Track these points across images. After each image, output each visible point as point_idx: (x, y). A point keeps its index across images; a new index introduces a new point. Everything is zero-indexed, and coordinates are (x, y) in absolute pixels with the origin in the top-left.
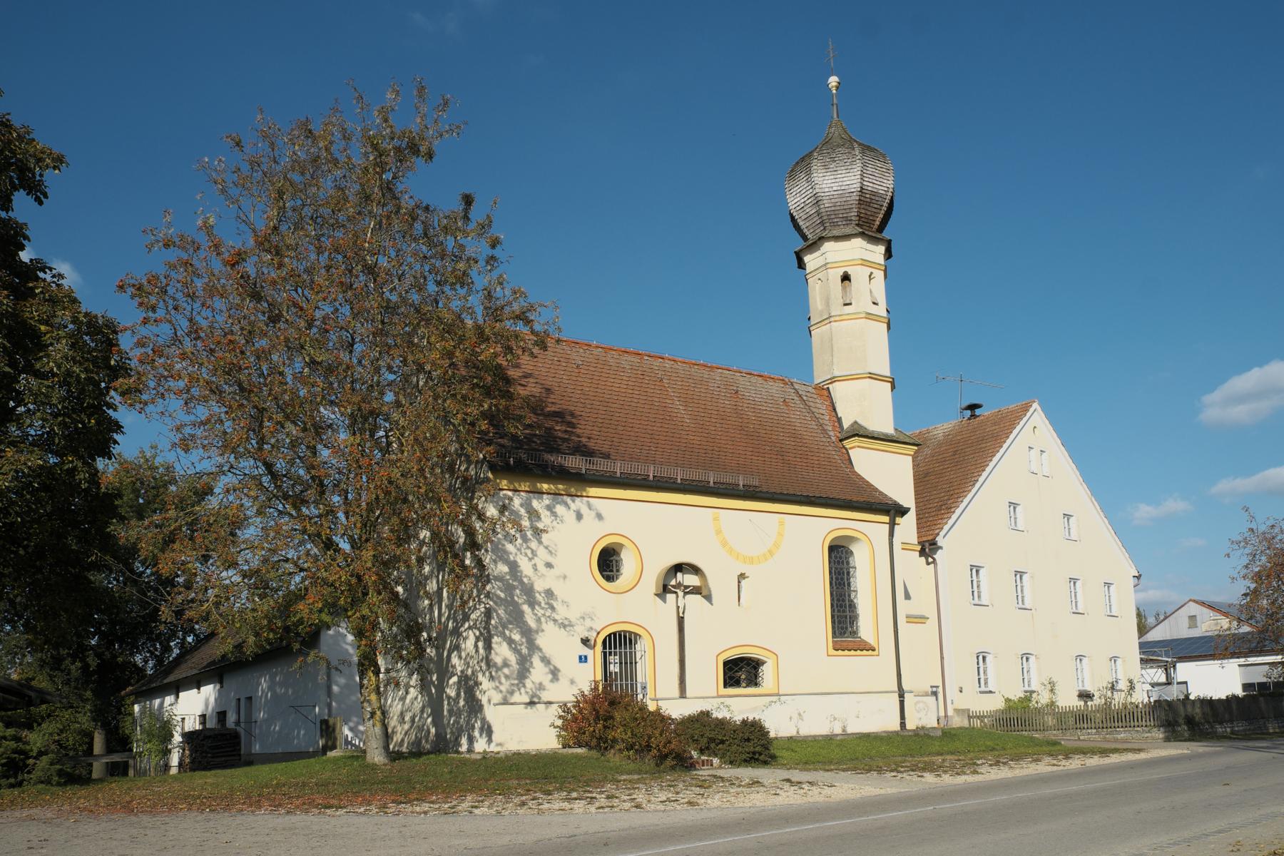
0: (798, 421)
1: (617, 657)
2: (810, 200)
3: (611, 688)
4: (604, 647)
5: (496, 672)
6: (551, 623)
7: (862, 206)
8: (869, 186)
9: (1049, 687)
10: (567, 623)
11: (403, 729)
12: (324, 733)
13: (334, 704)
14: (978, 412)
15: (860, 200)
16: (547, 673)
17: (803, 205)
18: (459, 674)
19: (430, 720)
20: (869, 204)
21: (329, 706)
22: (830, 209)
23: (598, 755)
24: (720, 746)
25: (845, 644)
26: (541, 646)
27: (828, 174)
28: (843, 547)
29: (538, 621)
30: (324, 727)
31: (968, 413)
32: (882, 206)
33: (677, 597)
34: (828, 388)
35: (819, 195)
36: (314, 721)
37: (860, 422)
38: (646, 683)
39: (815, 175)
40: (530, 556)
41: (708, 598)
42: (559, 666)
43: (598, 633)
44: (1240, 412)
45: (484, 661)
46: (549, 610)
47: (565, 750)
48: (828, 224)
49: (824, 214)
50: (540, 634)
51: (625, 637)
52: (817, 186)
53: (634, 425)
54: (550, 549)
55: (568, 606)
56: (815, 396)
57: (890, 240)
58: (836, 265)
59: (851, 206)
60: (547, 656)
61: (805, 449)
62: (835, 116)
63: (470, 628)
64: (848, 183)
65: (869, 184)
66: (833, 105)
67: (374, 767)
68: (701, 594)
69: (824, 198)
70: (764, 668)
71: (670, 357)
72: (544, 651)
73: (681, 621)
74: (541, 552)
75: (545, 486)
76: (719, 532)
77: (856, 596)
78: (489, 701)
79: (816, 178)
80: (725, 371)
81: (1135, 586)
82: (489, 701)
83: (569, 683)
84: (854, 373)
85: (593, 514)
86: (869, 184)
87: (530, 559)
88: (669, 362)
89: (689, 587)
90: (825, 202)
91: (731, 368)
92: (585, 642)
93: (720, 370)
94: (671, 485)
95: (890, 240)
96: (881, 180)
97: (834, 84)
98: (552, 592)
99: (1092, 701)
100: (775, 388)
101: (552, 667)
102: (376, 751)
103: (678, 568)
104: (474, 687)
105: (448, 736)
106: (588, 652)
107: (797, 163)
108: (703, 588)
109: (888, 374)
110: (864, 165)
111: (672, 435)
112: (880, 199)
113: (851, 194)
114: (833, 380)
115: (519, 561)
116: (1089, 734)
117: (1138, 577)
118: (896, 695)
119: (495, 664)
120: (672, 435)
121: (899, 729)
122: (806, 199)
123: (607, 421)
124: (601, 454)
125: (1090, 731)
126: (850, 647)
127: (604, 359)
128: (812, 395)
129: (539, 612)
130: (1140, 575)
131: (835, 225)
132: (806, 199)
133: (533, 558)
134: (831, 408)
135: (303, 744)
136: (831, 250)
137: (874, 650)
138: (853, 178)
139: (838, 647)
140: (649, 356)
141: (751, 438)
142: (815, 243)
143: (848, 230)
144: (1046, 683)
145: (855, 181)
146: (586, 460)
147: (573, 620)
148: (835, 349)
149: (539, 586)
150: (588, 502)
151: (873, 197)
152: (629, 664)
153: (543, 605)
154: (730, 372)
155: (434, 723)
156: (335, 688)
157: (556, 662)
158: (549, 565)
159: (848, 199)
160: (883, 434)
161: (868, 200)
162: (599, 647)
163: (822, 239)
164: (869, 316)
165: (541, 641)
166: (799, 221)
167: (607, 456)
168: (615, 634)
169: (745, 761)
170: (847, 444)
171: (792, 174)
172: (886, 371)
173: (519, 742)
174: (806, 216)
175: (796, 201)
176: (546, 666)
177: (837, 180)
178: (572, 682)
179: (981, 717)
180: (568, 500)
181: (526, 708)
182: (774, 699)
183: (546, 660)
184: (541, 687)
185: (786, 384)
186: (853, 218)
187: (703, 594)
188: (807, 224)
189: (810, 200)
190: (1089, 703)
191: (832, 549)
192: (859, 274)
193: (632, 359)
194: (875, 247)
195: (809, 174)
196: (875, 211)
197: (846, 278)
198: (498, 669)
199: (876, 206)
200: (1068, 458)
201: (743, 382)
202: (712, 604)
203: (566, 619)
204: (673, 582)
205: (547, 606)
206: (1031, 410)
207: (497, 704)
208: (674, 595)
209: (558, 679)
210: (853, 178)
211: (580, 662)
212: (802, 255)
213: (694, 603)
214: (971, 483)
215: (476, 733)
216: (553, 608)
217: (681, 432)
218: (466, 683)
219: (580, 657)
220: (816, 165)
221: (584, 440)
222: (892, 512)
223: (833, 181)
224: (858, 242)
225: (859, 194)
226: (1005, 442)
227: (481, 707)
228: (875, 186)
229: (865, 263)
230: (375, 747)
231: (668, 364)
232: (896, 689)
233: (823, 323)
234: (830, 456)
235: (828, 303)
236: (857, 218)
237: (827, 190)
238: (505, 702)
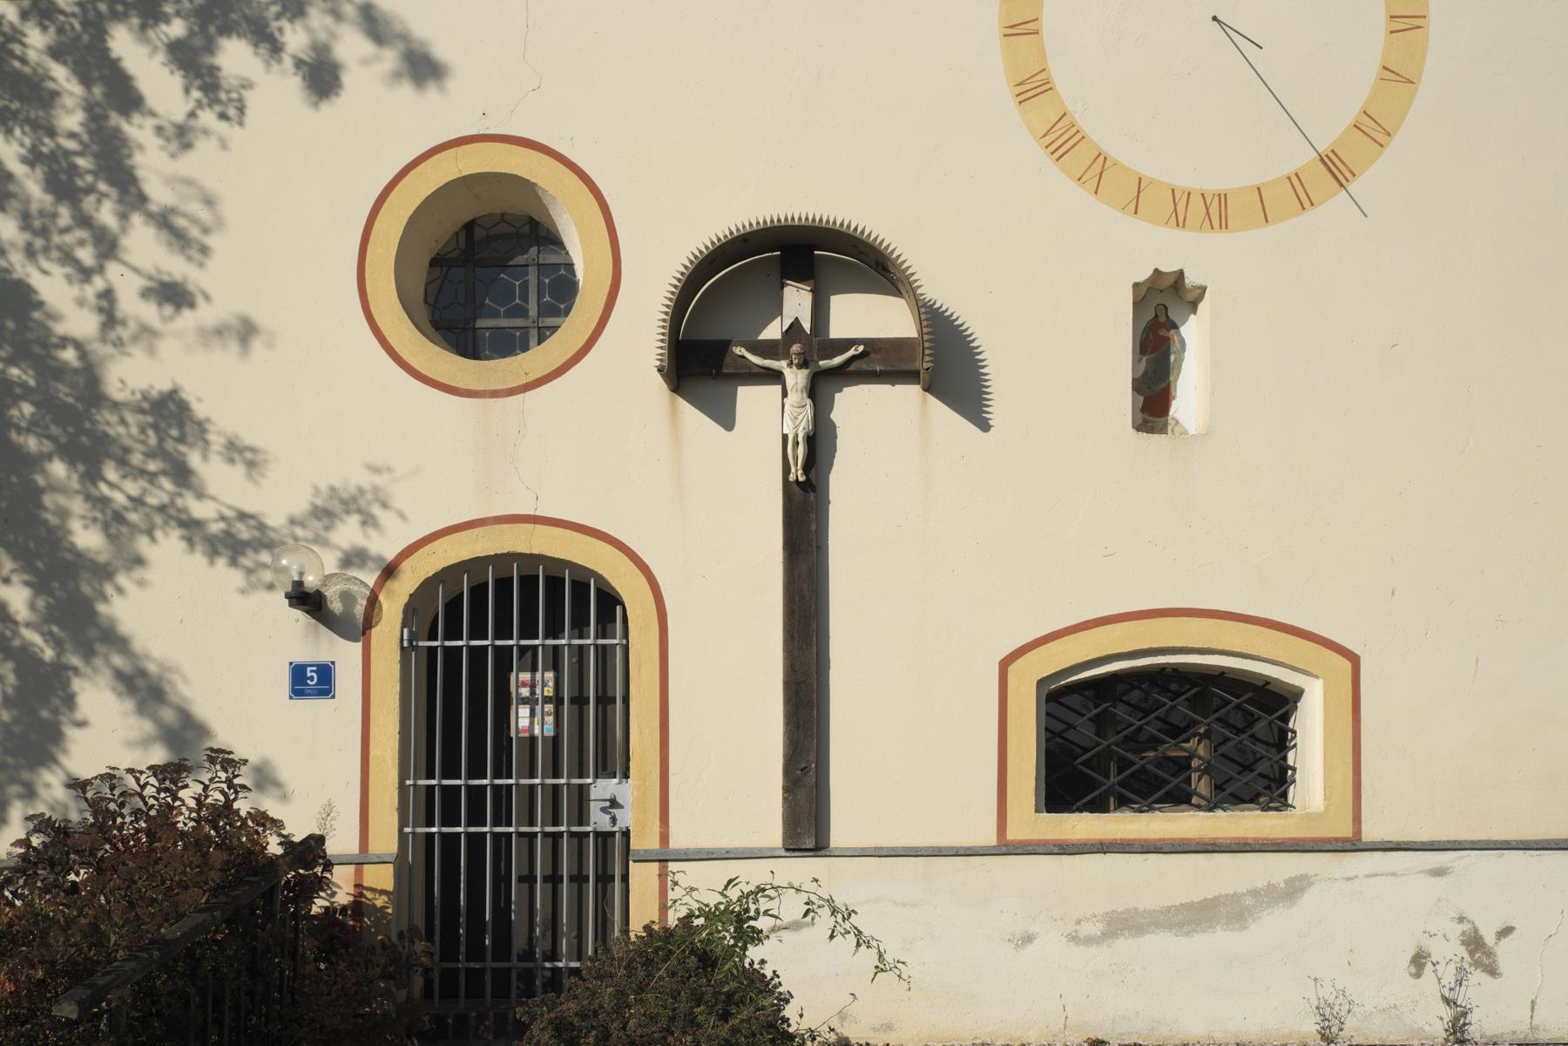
10: (244, 532)
29: (113, 521)
40: (86, 255)
46: (167, 484)
50: (122, 579)
54: (180, 222)
55: (251, 464)
60: (152, 668)
72: (138, 645)
85: (390, 58)
98: (184, 407)
129: (119, 488)
176: (142, 709)
202: (984, 426)
203: (243, 516)
216: (182, 475)
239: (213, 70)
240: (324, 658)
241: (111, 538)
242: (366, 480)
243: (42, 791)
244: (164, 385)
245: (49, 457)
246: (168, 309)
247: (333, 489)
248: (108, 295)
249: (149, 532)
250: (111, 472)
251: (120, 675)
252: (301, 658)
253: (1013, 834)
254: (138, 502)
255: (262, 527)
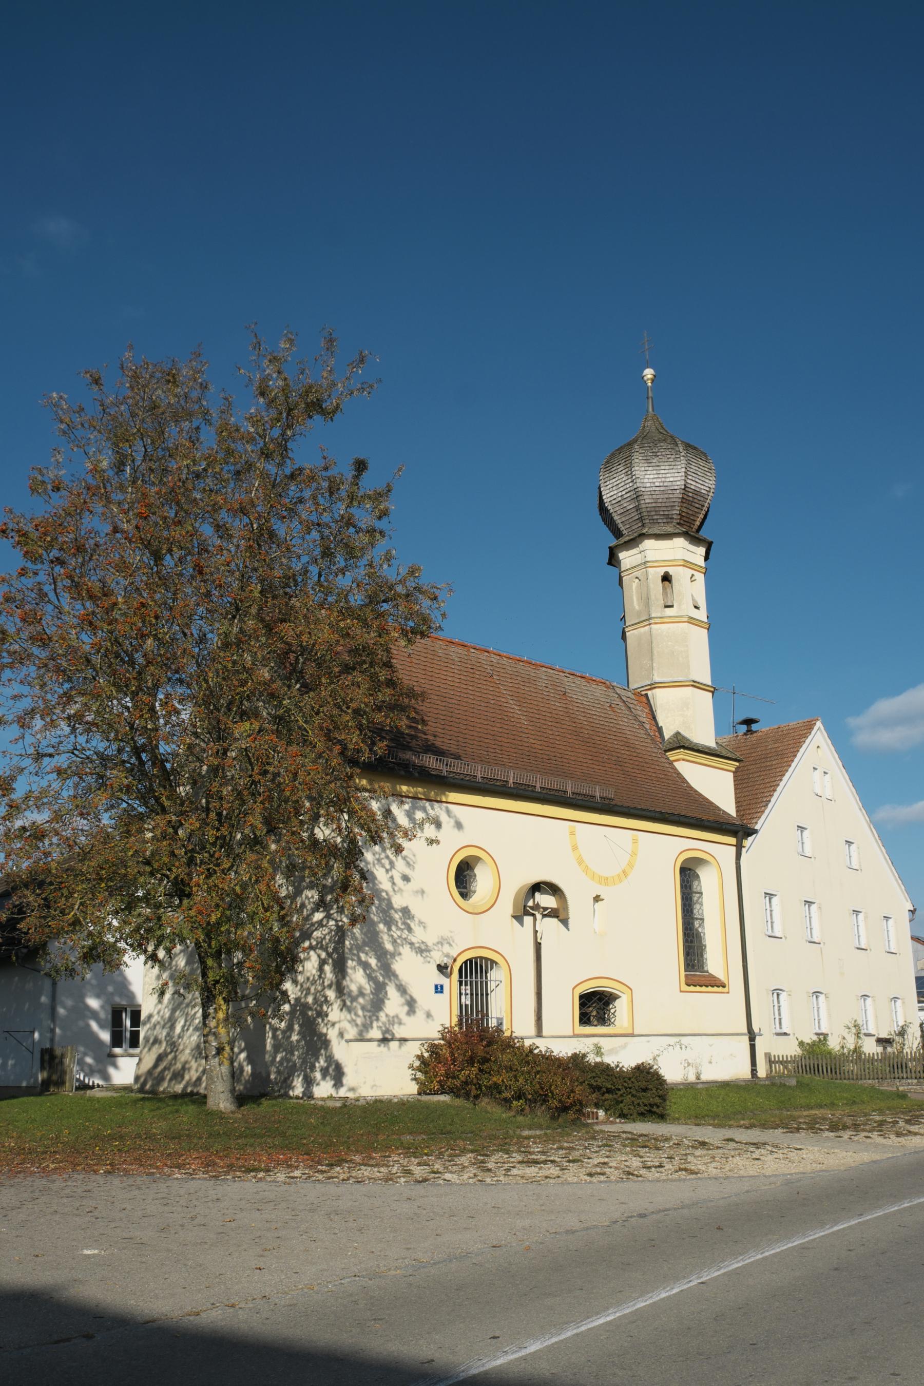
0: (628, 728)
1: (468, 987)
2: (628, 495)
3: (483, 1023)
4: (461, 976)
5: (352, 1002)
6: (407, 947)
7: (685, 505)
8: (693, 485)
9: (854, 1030)
10: (423, 947)
11: (199, 1065)
12: (46, 1065)
13: (58, 1031)
14: (754, 727)
15: (683, 498)
16: (403, 1005)
17: (620, 499)
18: (292, 1002)
19: (243, 1056)
20: (690, 503)
21: (52, 1031)
22: (650, 505)
23: (469, 1105)
24: (607, 1095)
25: (697, 979)
26: (398, 972)
27: (650, 468)
28: (690, 869)
29: (394, 942)
30: (47, 1057)
31: (744, 728)
32: (703, 506)
33: (535, 920)
34: (646, 695)
35: (639, 489)
36: (31, 1050)
37: (683, 733)
38: (502, 1019)
39: (637, 468)
40: (388, 867)
41: (565, 922)
42: (415, 996)
43: (455, 960)
44: (888, 738)
45: (334, 987)
46: (406, 931)
47: (425, 1098)
48: (647, 521)
49: (644, 510)
50: (397, 958)
51: (476, 963)
52: (638, 480)
53: (475, 724)
54: (408, 860)
55: (424, 927)
56: (635, 703)
57: (712, 542)
58: (657, 563)
59: (672, 504)
60: (403, 983)
61: (641, 760)
62: (650, 410)
63: (311, 947)
64: (671, 479)
65: (692, 483)
66: (648, 398)
67: (220, 1115)
68: (557, 917)
69: (645, 493)
70: (617, 1003)
71: (495, 651)
72: (400, 977)
73: (538, 947)
74: (400, 863)
75: (404, 788)
76: (575, 848)
77: (702, 925)
78: (341, 1035)
79: (637, 472)
80: (549, 670)
81: (910, 921)
82: (341, 1035)
83: (425, 1016)
84: (676, 679)
85: (452, 822)
86: (692, 483)
87: (387, 871)
88: (495, 656)
89: (547, 909)
90: (646, 497)
91: (554, 667)
92: (442, 968)
93: (544, 669)
94: (531, 794)
95: (712, 542)
96: (703, 479)
97: (649, 376)
98: (409, 911)
99: (892, 1046)
100: (599, 690)
101: (408, 997)
102: (221, 1095)
103: (537, 888)
104: (315, 1019)
105: (272, 1077)
106: (444, 981)
107: (613, 455)
108: (561, 910)
109: (710, 683)
110: (689, 462)
111: (512, 737)
112: (702, 499)
113: (674, 492)
114: (653, 686)
115: (375, 872)
116: (909, 1084)
117: (913, 912)
118: (746, 1038)
119: (350, 994)
120: (512, 737)
121: (750, 1077)
122: (624, 493)
123: (449, 719)
124: (452, 754)
125: (910, 1081)
126: (702, 983)
127: (432, 649)
128: (633, 701)
129: (396, 933)
130: (915, 910)
131: (654, 522)
132: (624, 493)
133: (391, 870)
134: (650, 717)
135: (12, 1077)
136: (653, 549)
137: (724, 986)
138: (676, 475)
139: (690, 982)
140: (474, 649)
141: (588, 744)
142: (697, 538)
143: (670, 529)
144: (851, 1025)
145: (679, 479)
146: (437, 759)
147: (430, 944)
148: (655, 652)
149: (398, 902)
150: (447, 808)
151: (695, 496)
152: (480, 996)
153: (400, 924)
154: (554, 672)
155: (249, 1059)
156: (61, 1011)
157: (414, 991)
158: (406, 878)
159: (671, 496)
160: (703, 746)
161: (691, 499)
162: (455, 975)
163: (642, 536)
164: (692, 621)
165: (398, 966)
166: (613, 515)
167: (458, 757)
168: (471, 960)
169: (642, 1114)
170: (672, 756)
171: (609, 465)
172: (707, 680)
173: (372, 1087)
174: (622, 511)
175: (612, 493)
176: (402, 996)
177: (660, 476)
178: (429, 1015)
179: (784, 1063)
180: (427, 804)
181: (379, 1046)
182: (672, 1040)
183: (402, 989)
184: (396, 1020)
185: (607, 687)
186: (675, 517)
187: (561, 917)
188: (624, 519)
189: (628, 495)
190: (889, 1049)
191: (683, 870)
192: (680, 575)
193: (460, 651)
194: (696, 548)
195: (629, 466)
196: (696, 510)
197: (666, 578)
198: (354, 999)
199: (697, 505)
200: (849, 781)
201: (568, 682)
202: (569, 930)
203: (423, 942)
204: (530, 903)
205: (403, 927)
206: (816, 728)
207: (351, 1041)
208: (531, 918)
209: (414, 1012)
210: (676, 475)
211: (436, 992)
212: (616, 551)
213: (549, 926)
214: (764, 804)
215: (318, 1075)
216: (410, 929)
217: (521, 734)
218: (304, 1014)
219: (436, 986)
220: (637, 458)
221: (431, 738)
222: (740, 834)
223: (656, 476)
224: (680, 542)
225: (682, 491)
226: (793, 761)
227: (326, 1043)
228: (697, 485)
229: (687, 564)
230: (222, 1090)
231: (495, 659)
232: (746, 1031)
233: (642, 625)
234: (665, 769)
235: (648, 604)
236: (679, 517)
237: (648, 485)
238: (361, 1039)
239: (415, 819)
240: (441, 983)
241: (394, 946)
242: (449, 935)
243: (380, 1018)
244: (405, 905)
245: (379, 923)
246: (405, 882)
247: (442, 937)
248: (392, 877)
249: (402, 946)
250: (394, 928)
251: (396, 985)
252: (437, 983)
253: (576, 1032)
254: (400, 937)
255: (427, 946)
